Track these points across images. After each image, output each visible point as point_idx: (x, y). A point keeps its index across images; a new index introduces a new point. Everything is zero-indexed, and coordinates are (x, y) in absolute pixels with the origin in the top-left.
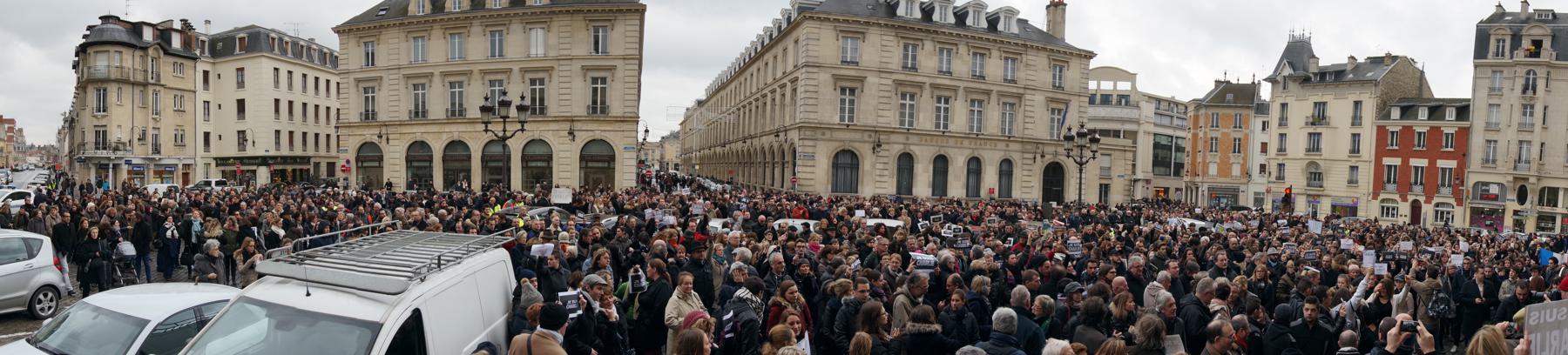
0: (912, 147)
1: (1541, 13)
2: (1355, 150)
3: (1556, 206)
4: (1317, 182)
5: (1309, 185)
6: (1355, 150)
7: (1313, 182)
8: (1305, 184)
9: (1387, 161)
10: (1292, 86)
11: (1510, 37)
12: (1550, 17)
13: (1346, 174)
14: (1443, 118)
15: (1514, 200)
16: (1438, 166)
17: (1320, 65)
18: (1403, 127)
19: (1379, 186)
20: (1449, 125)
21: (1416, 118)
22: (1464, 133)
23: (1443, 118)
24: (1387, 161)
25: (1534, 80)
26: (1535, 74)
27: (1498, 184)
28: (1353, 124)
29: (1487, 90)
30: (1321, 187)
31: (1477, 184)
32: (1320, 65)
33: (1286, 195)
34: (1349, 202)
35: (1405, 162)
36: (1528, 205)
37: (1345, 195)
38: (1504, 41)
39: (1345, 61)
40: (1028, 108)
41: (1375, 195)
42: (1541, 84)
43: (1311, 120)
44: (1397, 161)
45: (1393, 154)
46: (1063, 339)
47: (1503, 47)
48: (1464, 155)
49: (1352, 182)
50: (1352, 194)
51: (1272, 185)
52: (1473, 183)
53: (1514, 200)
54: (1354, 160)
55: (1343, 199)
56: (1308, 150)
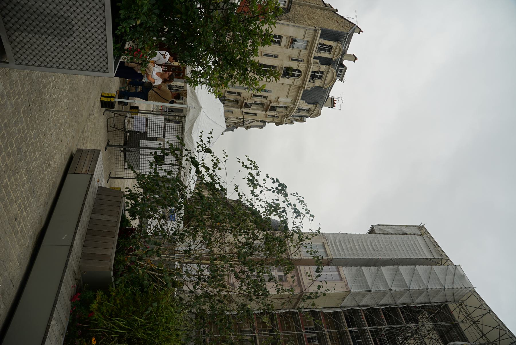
1: (343, 72)
25: (293, 75)
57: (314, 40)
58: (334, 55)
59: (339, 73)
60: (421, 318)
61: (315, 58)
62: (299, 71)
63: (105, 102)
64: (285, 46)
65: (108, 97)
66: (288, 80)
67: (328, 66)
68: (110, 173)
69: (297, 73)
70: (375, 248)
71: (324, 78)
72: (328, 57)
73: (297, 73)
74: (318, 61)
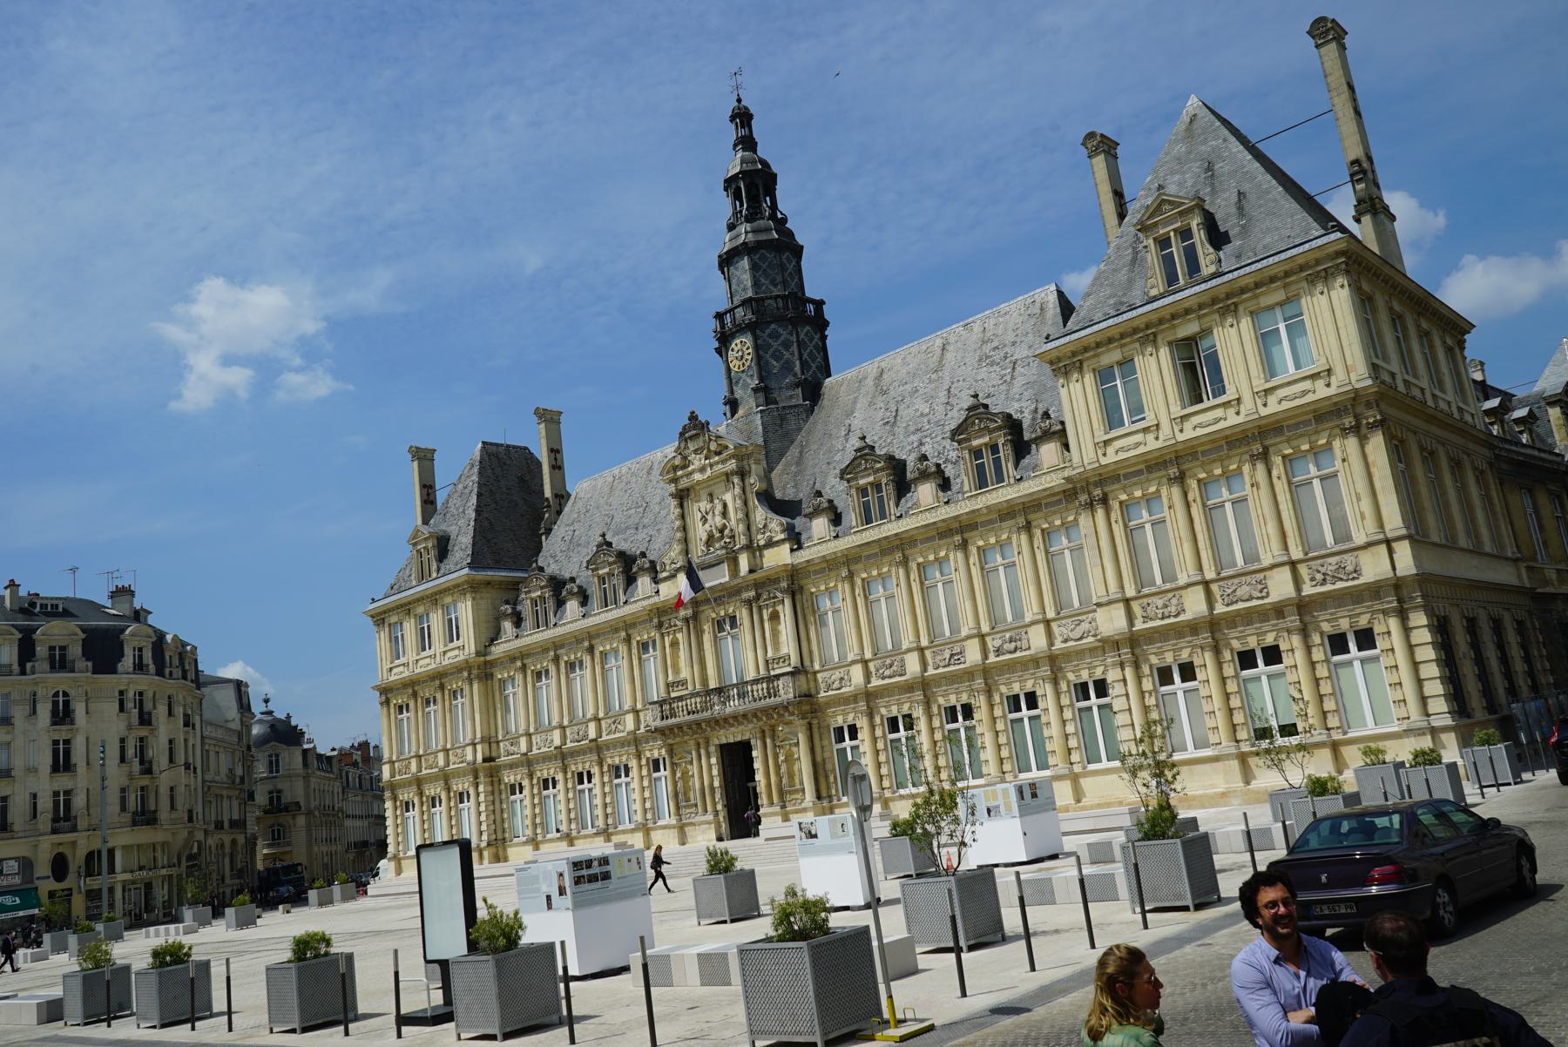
12: (60, 610)
15: (49, 877)
42: (79, 709)
53: (49, 877)
59: (49, 609)
64: (8, 733)
69: (61, 699)
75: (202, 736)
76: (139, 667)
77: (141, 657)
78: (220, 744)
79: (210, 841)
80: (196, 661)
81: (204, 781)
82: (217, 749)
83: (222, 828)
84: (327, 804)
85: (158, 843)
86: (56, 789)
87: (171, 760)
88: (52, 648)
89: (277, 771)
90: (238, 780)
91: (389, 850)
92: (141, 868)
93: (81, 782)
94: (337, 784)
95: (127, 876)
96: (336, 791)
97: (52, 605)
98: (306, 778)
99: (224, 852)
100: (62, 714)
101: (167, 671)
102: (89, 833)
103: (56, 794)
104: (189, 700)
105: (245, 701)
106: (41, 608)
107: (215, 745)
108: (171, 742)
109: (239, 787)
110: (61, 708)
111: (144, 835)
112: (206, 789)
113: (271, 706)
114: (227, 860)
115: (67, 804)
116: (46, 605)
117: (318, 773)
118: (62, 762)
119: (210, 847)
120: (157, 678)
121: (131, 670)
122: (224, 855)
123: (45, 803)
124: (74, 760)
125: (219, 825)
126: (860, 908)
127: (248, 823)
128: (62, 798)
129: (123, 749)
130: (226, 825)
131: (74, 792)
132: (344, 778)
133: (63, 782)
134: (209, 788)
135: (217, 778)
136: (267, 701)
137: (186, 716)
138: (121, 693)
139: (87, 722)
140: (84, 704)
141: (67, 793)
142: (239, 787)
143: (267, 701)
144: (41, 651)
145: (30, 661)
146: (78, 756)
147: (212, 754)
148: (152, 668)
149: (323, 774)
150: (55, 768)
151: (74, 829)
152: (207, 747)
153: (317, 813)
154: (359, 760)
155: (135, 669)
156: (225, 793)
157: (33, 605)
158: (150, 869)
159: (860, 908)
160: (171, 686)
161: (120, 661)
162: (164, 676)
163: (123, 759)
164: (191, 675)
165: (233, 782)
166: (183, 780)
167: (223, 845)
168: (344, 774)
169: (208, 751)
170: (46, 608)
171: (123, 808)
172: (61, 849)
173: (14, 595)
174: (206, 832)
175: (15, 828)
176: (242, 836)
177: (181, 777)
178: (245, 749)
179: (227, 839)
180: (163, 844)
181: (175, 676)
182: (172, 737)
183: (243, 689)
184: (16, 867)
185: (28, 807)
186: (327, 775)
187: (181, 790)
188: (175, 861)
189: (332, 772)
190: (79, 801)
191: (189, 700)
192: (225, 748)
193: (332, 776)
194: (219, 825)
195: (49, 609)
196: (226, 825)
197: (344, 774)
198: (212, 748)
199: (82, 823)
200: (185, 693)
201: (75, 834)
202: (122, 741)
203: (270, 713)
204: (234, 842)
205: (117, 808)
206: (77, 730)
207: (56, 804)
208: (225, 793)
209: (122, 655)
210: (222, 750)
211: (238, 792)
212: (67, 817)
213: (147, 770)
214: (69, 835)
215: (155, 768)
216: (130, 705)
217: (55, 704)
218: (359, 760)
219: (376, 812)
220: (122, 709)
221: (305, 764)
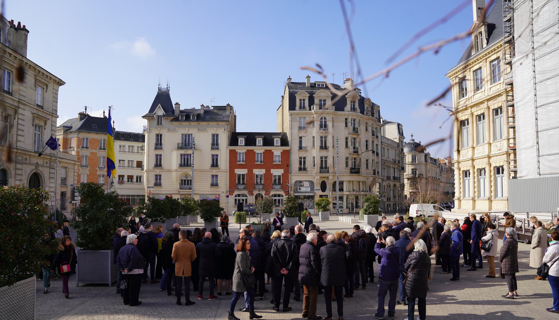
0: (41, 169)
1: (319, 83)
2: (215, 164)
3: (343, 191)
4: (186, 186)
5: (181, 189)
6: (215, 164)
7: (183, 186)
8: (178, 187)
9: (238, 171)
10: (164, 122)
11: (308, 98)
12: (325, 86)
13: (210, 181)
14: (255, 145)
15: (319, 190)
16: (254, 172)
17: (180, 109)
18: (247, 150)
19: (233, 187)
20: (277, 151)
21: (255, 145)
22: (286, 155)
23: (255, 145)
24: (238, 171)
25: (325, 122)
26: (325, 118)
27: (309, 181)
28: (156, 148)
29: (297, 128)
30: (190, 189)
31: (296, 182)
32: (180, 109)
33: (22, 199)
34: (212, 197)
35: (250, 172)
36: (327, 191)
37: (210, 193)
38: (304, 100)
39: (199, 108)
40: (20, 133)
41: (231, 192)
42: (330, 124)
43: (180, 145)
44: (244, 171)
45: (241, 167)
46: (346, 292)
47: (304, 103)
48: (288, 166)
49: (214, 185)
50: (215, 193)
51: (151, 189)
52: (295, 181)
53: (319, 190)
54: (214, 171)
55: (208, 196)
56: (181, 166)
57: (298, 114)
58: (306, 96)
59: (321, 86)
60: (280, 229)
61: (310, 110)
62: (322, 118)
63: (280, 201)
64: (305, 133)
65: (35, 137)
66: (329, 126)
67: (315, 98)
68: (24, 120)
69: (323, 120)
70: (528, 82)
71: (324, 98)
72: (308, 100)
73: (323, 120)
74: (312, 107)
75: (381, 142)
76: (353, 109)
77: (354, 105)
78: (390, 146)
79: (384, 184)
80: (379, 111)
81: (382, 160)
82: (388, 148)
83: (390, 179)
84: (434, 176)
85: (361, 181)
86: (322, 155)
87: (367, 149)
88: (320, 101)
89: (415, 162)
90: (397, 162)
91: (455, 195)
92: (354, 191)
93: (330, 154)
94: (438, 169)
95: (348, 193)
96: (437, 172)
97: (322, 85)
98: (426, 165)
99: (390, 189)
100: (324, 126)
101: (365, 112)
102: (333, 174)
103: (322, 158)
104: (375, 126)
105: (401, 132)
106: (318, 86)
107: (387, 146)
108: (367, 141)
109: (398, 164)
110: (323, 124)
111: (355, 178)
112: (383, 163)
113: (414, 138)
114: (392, 192)
115: (326, 161)
116: (320, 85)
117: (431, 164)
118: (324, 147)
119: (384, 186)
120: (360, 114)
121: (350, 110)
122: (391, 190)
123: (318, 162)
124: (328, 145)
125: (388, 178)
126: (104, 115)
127: (401, 179)
128: (324, 159)
129: (347, 142)
130: (392, 178)
131: (328, 157)
132: (441, 168)
133: (324, 153)
134: (384, 163)
135: (388, 160)
136: (412, 136)
137: (373, 131)
138: (346, 119)
139: (333, 130)
140: (332, 123)
141: (326, 157)
142: (398, 164)
143: (412, 136)
144: (316, 101)
145: (312, 105)
146: (329, 144)
147: (386, 150)
148: (358, 110)
149: (433, 165)
150: (321, 148)
151: (328, 172)
152: (383, 146)
153: (430, 179)
154: (447, 163)
155: (351, 110)
156: (391, 165)
157: (315, 84)
158: (357, 192)
159: (104, 115)
160: (365, 118)
161: (345, 106)
162: (364, 114)
163: (347, 146)
164: (376, 115)
165: (395, 162)
166: (371, 157)
167: (390, 186)
168: (441, 166)
169: (384, 148)
170: (320, 86)
171: (347, 166)
172: (324, 179)
173: (308, 81)
174: (383, 180)
175: (308, 169)
176: (399, 183)
177: (370, 156)
178: (400, 150)
179: (392, 184)
180: (363, 182)
181: (368, 114)
182: (367, 139)
183: (400, 126)
184: (308, 184)
185: (312, 162)
186: (434, 166)
187: (370, 161)
188: (368, 189)
189: (436, 165)
190: (330, 162)
191: (375, 126)
192: (392, 148)
193: (436, 166)
194: (388, 178)
195: (321, 86)
196: (392, 178)
197: (441, 166)
198: (386, 147)
199: (331, 170)
200: (373, 122)
201: (328, 174)
202: (347, 139)
203: (413, 140)
204: (395, 185)
205: (344, 165)
206: (329, 133)
207: (322, 161)
208: (391, 165)
209: (346, 104)
210: (390, 148)
211: (397, 166)
212: (326, 167)
213: (356, 152)
214: (326, 174)
215: (359, 151)
216: (349, 124)
217: (321, 122)
218: (447, 163)
219: (452, 182)
220: (346, 125)
221: (426, 160)
